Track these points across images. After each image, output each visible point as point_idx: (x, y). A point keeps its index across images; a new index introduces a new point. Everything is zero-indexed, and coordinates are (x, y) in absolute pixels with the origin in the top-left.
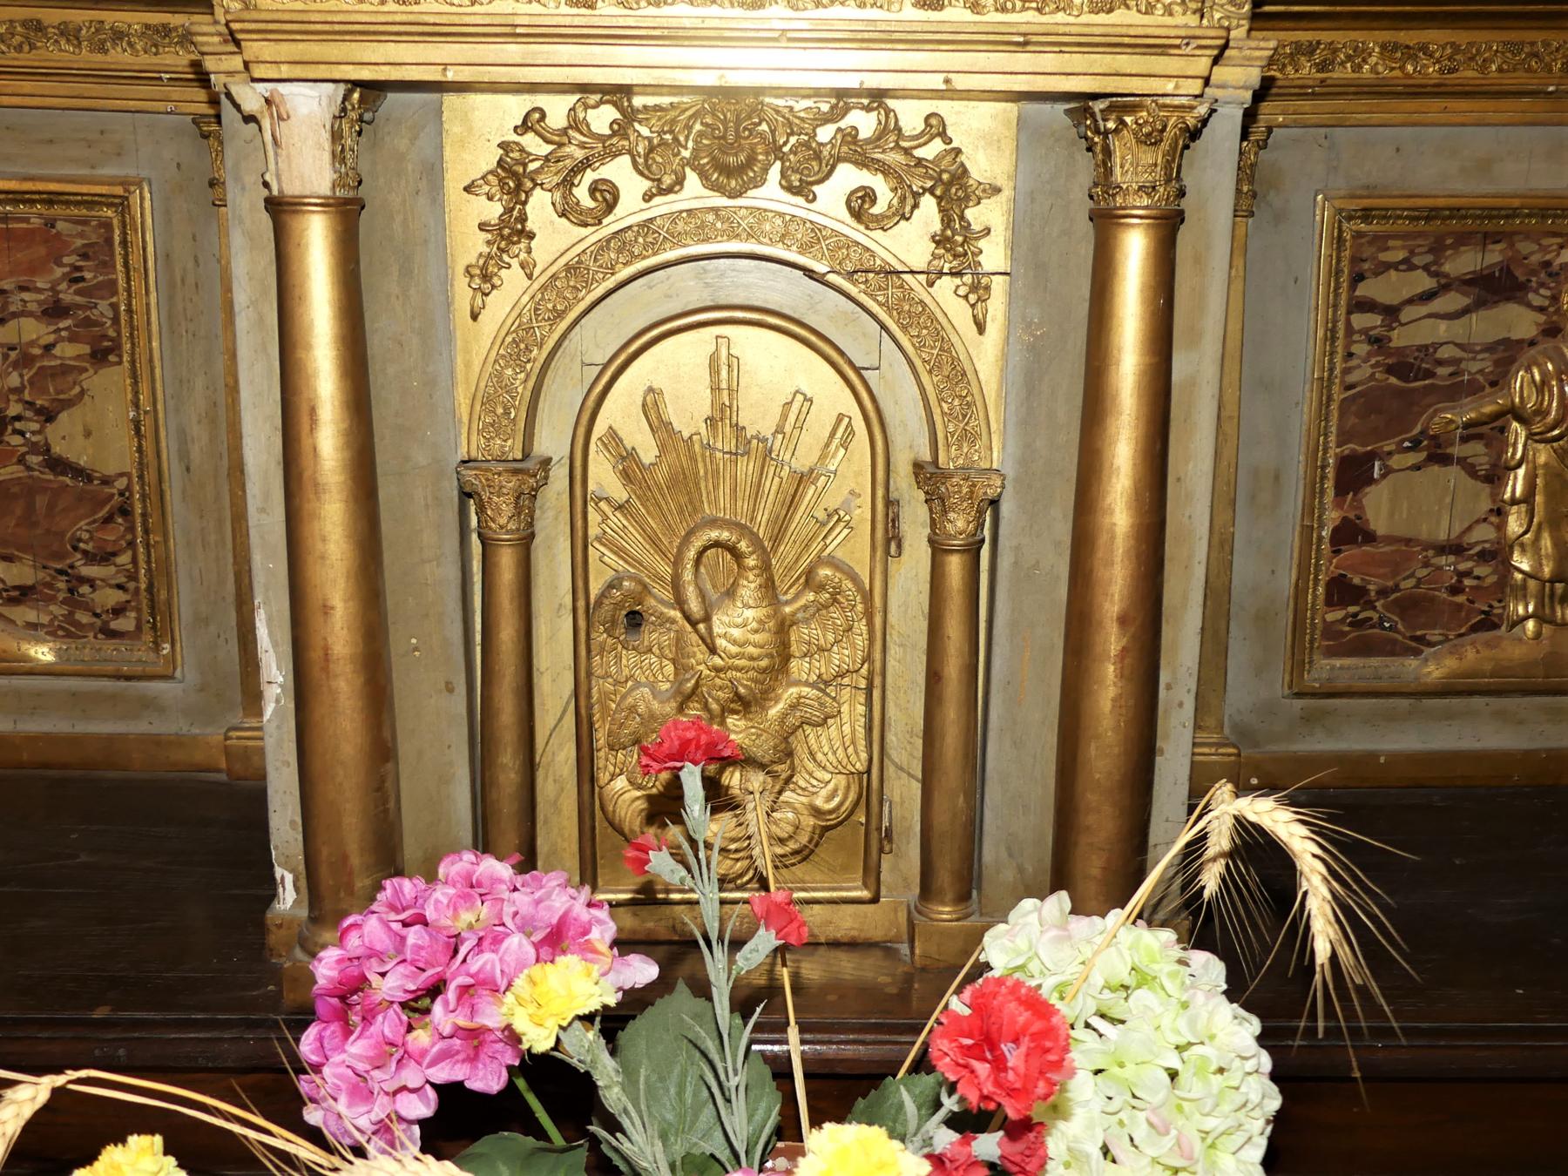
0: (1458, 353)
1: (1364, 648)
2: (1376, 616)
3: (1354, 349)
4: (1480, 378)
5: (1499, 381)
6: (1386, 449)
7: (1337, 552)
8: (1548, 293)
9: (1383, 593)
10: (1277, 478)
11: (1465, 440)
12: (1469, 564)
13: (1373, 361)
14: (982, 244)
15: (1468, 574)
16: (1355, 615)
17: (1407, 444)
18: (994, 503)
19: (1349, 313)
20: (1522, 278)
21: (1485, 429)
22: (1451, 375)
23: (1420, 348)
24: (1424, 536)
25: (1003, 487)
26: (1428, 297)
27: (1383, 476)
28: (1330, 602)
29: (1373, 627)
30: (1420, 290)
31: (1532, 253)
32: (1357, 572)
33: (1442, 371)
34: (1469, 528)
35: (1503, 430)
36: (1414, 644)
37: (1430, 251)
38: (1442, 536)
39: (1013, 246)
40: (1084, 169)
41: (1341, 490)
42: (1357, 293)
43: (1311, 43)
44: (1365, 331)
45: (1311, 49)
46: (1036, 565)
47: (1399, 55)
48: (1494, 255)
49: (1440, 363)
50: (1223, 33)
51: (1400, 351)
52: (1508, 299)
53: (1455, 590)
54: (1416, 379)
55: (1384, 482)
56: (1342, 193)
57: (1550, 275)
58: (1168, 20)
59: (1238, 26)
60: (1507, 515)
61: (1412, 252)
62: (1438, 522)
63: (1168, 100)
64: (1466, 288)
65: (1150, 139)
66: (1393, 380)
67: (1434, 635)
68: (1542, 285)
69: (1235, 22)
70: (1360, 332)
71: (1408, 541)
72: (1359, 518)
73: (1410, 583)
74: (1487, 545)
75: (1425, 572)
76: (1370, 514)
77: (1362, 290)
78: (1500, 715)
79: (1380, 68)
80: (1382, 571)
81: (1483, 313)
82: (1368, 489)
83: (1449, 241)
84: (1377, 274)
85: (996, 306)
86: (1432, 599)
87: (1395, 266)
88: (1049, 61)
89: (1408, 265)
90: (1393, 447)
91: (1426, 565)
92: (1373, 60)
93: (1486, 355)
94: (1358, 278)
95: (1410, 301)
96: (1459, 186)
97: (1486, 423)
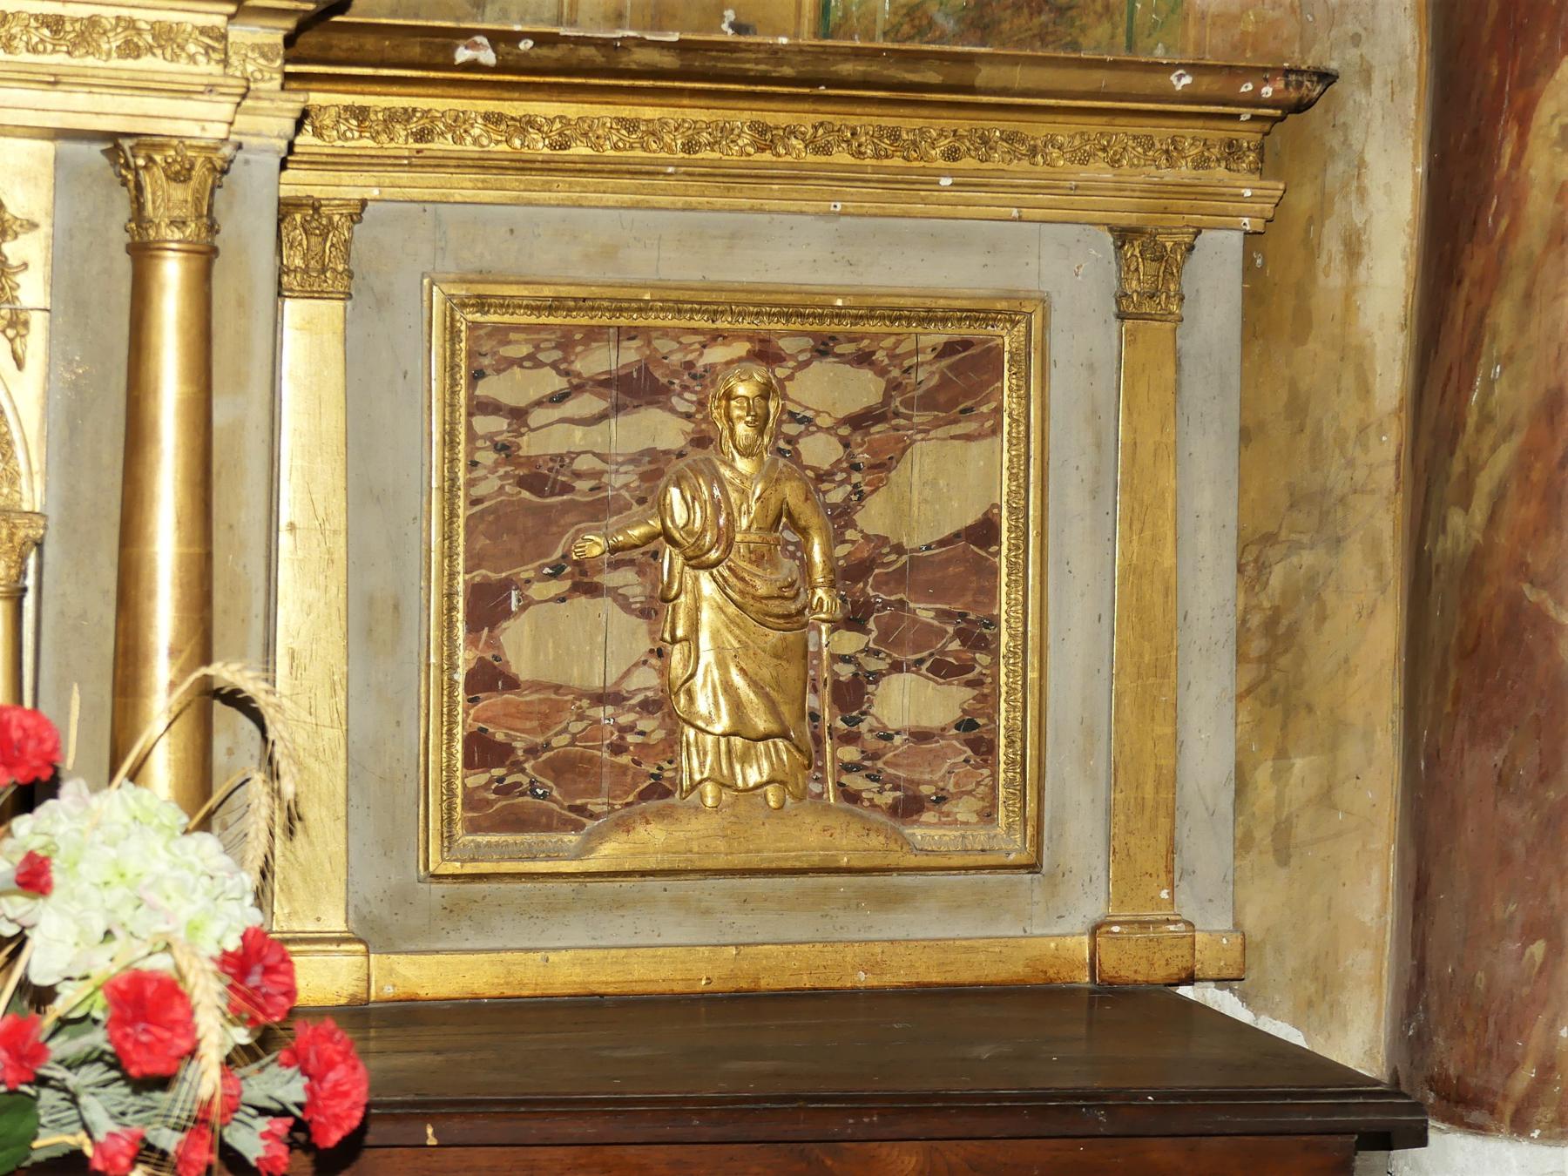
0: (599, 465)
1: (515, 822)
2: (525, 781)
3: (478, 457)
4: (627, 495)
5: (650, 498)
6: (524, 576)
7: (473, 701)
8: (694, 398)
9: (532, 751)
10: (396, 607)
11: (615, 565)
12: (631, 717)
13: (501, 471)
14: (19, 278)
15: (631, 728)
16: (501, 780)
17: (547, 570)
18: (39, 545)
19: (470, 414)
20: (664, 380)
21: (636, 554)
22: (592, 490)
23: (553, 458)
24: (576, 682)
25: (45, 527)
26: (559, 398)
27: (523, 609)
28: (469, 764)
29: (523, 794)
30: (548, 391)
31: (671, 352)
32: (499, 726)
33: (582, 485)
34: (627, 673)
35: (655, 555)
36: (573, 816)
37: (558, 346)
38: (597, 683)
39: (53, 283)
40: (122, 198)
41: (473, 626)
42: (478, 392)
43: (405, 110)
44: (490, 437)
45: (408, 114)
46: (83, 615)
47: (503, 127)
48: (631, 354)
49: (578, 475)
50: (244, 83)
51: (531, 461)
52: (650, 403)
53: (618, 749)
54: (552, 494)
55: (523, 616)
56: (452, 276)
57: (694, 377)
58: (192, 68)
59: (271, 79)
60: (670, 655)
61: (537, 347)
62: (591, 667)
63: (194, 142)
64: (601, 390)
65: (180, 175)
66: (526, 494)
67: (597, 804)
68: (685, 388)
69: (267, 76)
70: (484, 437)
71: (557, 688)
72: (496, 658)
73: (564, 739)
74: (650, 694)
75: (579, 726)
76: (510, 655)
77: (484, 389)
78: (680, 903)
79: (485, 141)
80: (528, 725)
81: (621, 419)
82: (505, 625)
83: (578, 336)
84: (498, 371)
85: (36, 343)
86: (591, 760)
87: (519, 362)
88: (80, 100)
89: (533, 361)
90: (531, 574)
91: (581, 717)
92: (476, 132)
93: (631, 468)
94: (477, 375)
95: (539, 403)
96: (582, 274)
97: (636, 546)
